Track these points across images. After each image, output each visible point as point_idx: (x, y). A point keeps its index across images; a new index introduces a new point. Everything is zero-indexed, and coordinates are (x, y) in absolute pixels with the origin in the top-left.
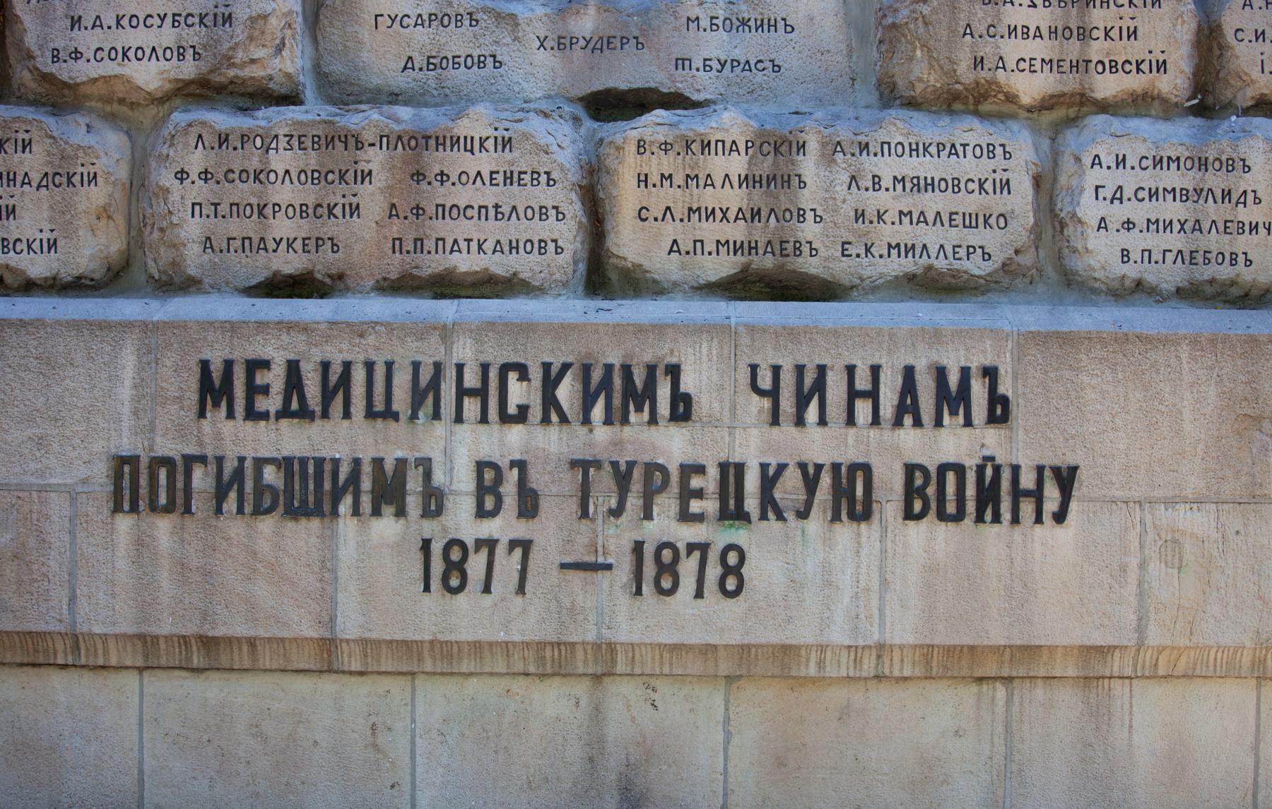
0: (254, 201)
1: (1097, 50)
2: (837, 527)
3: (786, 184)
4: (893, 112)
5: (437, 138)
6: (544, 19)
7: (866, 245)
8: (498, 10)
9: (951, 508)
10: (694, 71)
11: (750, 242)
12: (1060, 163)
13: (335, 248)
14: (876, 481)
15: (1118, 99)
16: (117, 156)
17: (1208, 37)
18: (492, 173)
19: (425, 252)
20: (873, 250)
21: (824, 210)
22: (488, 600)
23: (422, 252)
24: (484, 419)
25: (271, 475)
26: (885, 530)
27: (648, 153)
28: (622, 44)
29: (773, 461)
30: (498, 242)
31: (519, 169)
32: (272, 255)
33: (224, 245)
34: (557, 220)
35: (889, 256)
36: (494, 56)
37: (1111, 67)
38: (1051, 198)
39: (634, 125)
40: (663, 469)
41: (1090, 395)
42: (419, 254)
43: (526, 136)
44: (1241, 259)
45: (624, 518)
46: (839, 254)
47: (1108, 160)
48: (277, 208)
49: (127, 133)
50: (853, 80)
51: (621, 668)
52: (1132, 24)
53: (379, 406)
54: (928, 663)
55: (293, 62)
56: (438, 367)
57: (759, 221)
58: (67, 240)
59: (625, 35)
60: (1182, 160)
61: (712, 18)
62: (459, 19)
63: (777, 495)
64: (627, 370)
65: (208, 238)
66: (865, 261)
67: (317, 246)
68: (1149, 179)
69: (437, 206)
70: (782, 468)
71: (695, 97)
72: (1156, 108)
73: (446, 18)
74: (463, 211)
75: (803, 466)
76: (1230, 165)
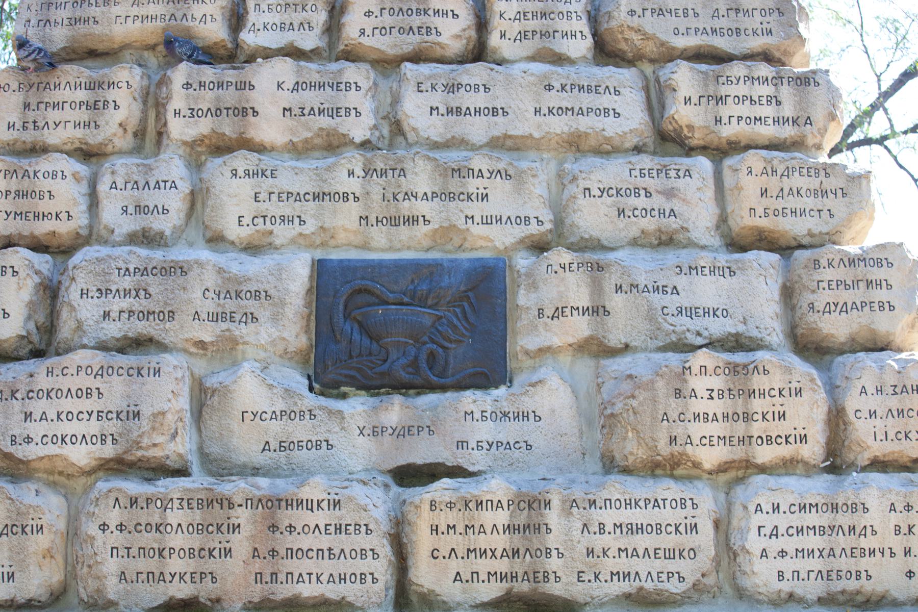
0: (156, 546)
1: (757, 428)
3: (537, 531)
4: (612, 477)
5: (287, 500)
6: (363, 414)
7: (595, 573)
8: (330, 408)
10: (470, 450)
11: (512, 573)
12: (733, 511)
13: (214, 580)
15: (773, 463)
16: (57, 513)
17: (836, 417)
18: (326, 525)
19: (279, 582)
20: (600, 577)
21: (565, 549)
23: (276, 583)
27: (438, 510)
28: (418, 431)
30: (331, 575)
31: (346, 523)
32: (168, 584)
33: (135, 578)
34: (374, 559)
35: (612, 581)
36: (327, 441)
37: (767, 440)
38: (727, 536)
39: (427, 490)
42: (274, 584)
43: (350, 499)
44: (864, 575)
46: (576, 580)
47: (767, 507)
48: (172, 551)
49: (65, 496)
50: (584, 454)
52: (781, 410)
55: (183, 445)
57: (518, 558)
58: (22, 573)
59: (421, 425)
60: (820, 505)
61: (482, 412)
62: (302, 414)
65: (123, 573)
66: (594, 585)
67: (201, 578)
68: (799, 519)
69: (287, 549)
71: (471, 469)
72: (800, 469)
73: (293, 414)
76: (854, 508)
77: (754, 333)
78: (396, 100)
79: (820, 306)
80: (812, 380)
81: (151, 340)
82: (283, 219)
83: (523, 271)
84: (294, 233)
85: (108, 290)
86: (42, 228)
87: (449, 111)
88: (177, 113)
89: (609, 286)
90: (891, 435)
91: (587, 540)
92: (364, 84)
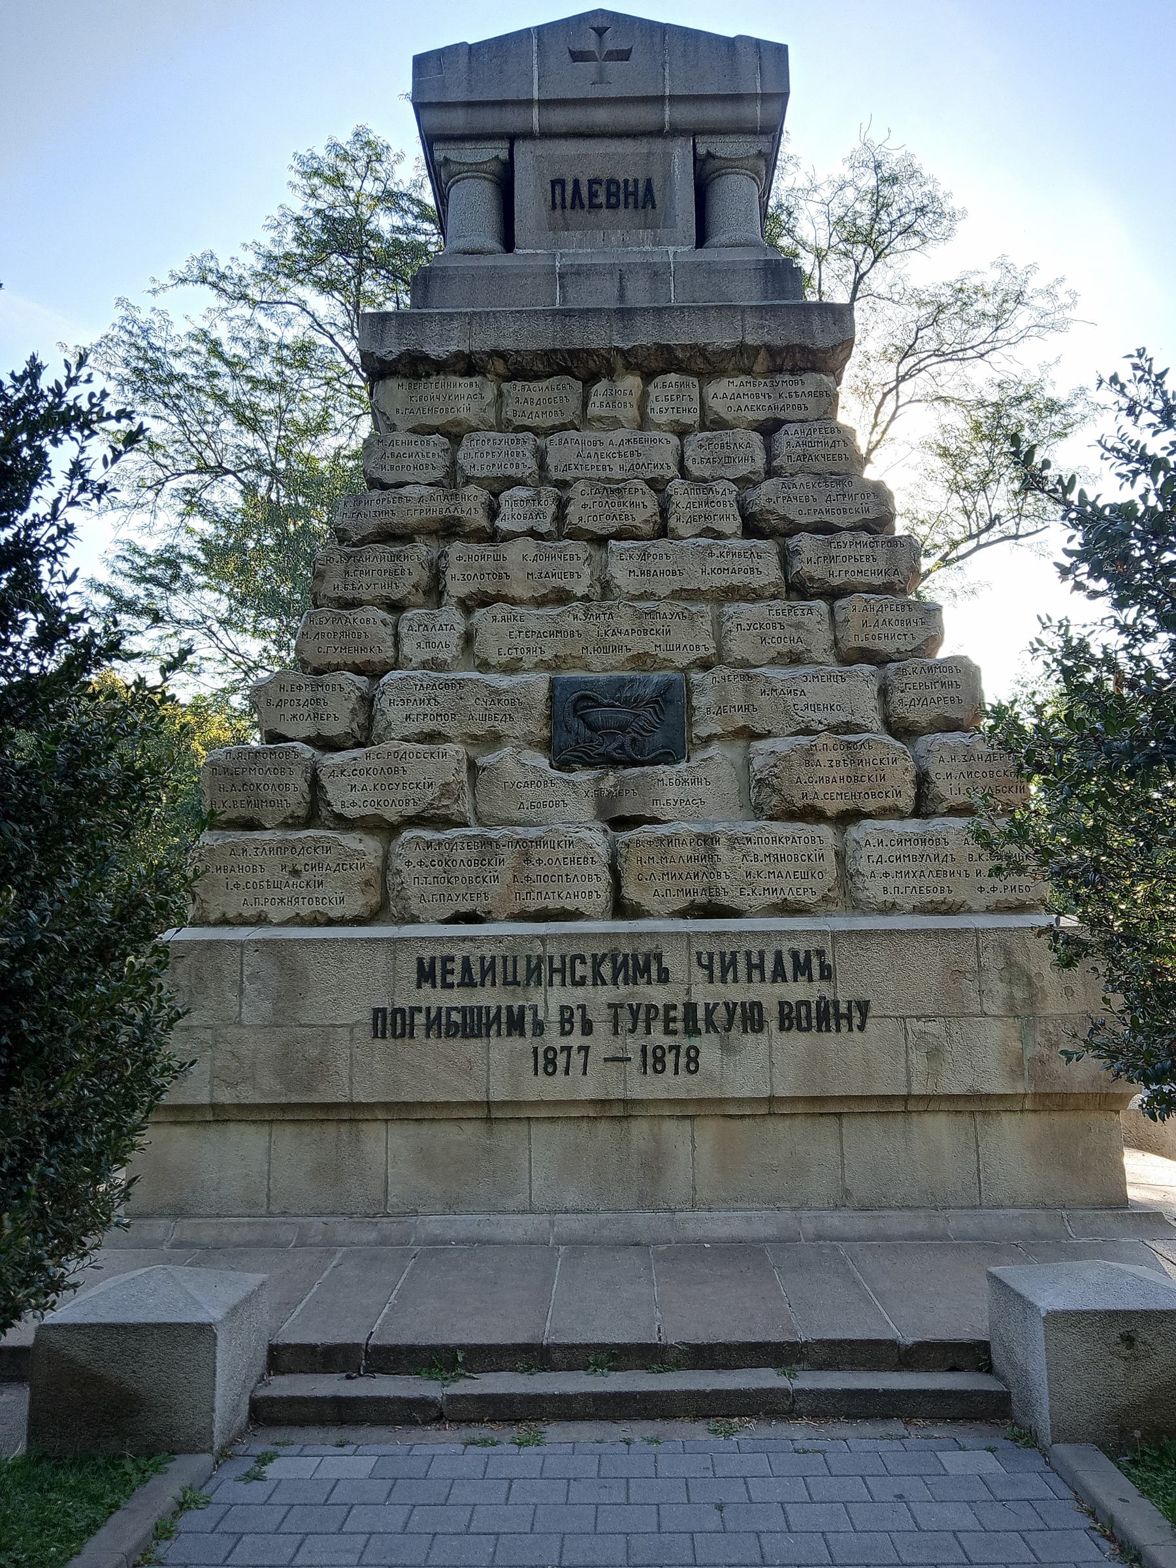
25: (456, 1017)
40: (655, 1007)
53: (510, 979)
64: (635, 957)
68: (898, 851)
75: (726, 1004)
79: (907, 701)
81: (440, 733)
86: (360, 658)
91: (747, 865)
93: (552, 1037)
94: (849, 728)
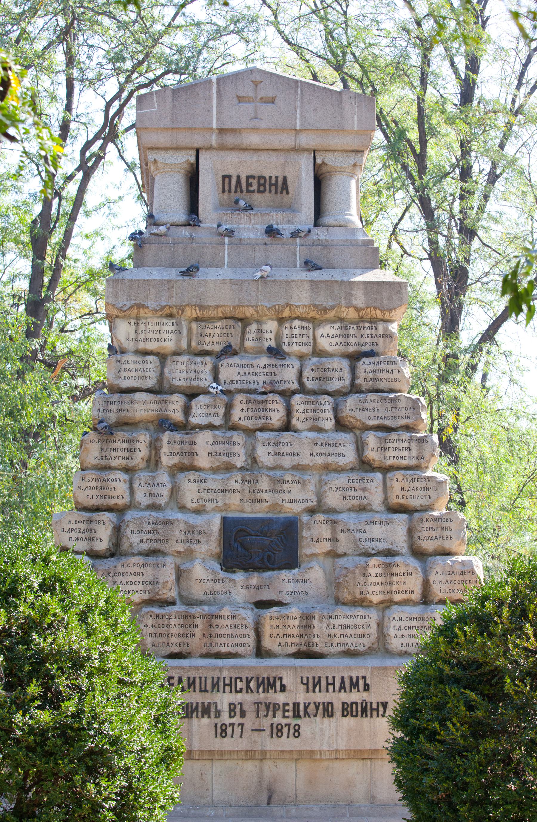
1: (394, 588)
2: (324, 719)
4: (338, 607)
9: (354, 714)
14: (334, 707)
22: (232, 739)
24: (231, 692)
26: (337, 719)
29: (307, 702)
40: (278, 704)
41: (391, 683)
43: (239, 615)
45: (268, 717)
51: (268, 757)
53: (203, 689)
54: (349, 755)
56: (218, 678)
62: (219, 580)
63: (308, 711)
64: (268, 679)
66: (331, 648)
68: (408, 624)
70: (309, 704)
71: (284, 602)
74: (222, 636)
75: (315, 703)
77: (396, 549)
78: (254, 448)
79: (422, 537)
80: (416, 569)
81: (159, 551)
82: (209, 500)
83: (305, 522)
84: (214, 506)
85: (142, 531)
87: (276, 454)
88: (165, 454)
89: (339, 530)
90: (447, 591)
91: (328, 631)
92: (241, 443)
93: (225, 718)
94: (389, 553)
